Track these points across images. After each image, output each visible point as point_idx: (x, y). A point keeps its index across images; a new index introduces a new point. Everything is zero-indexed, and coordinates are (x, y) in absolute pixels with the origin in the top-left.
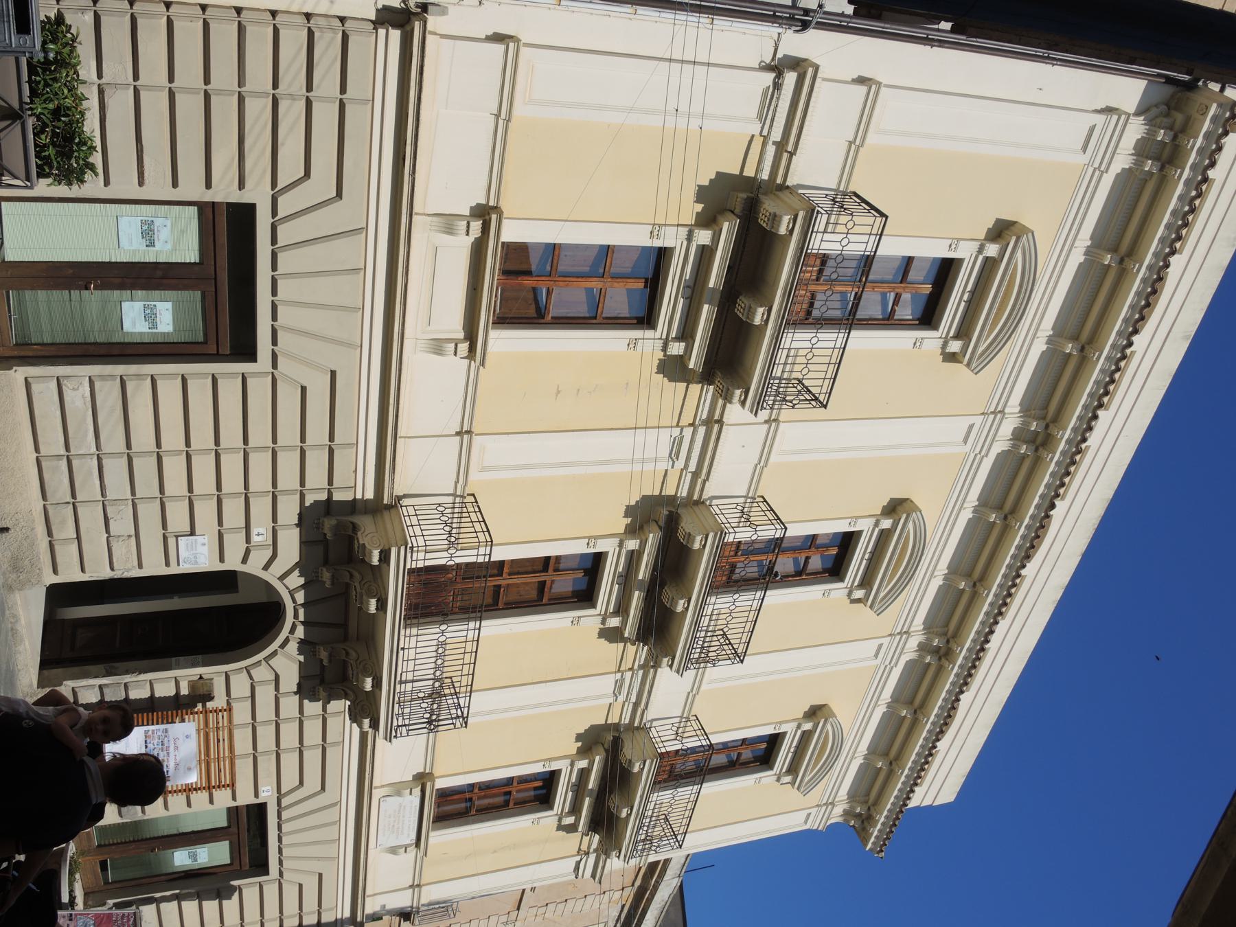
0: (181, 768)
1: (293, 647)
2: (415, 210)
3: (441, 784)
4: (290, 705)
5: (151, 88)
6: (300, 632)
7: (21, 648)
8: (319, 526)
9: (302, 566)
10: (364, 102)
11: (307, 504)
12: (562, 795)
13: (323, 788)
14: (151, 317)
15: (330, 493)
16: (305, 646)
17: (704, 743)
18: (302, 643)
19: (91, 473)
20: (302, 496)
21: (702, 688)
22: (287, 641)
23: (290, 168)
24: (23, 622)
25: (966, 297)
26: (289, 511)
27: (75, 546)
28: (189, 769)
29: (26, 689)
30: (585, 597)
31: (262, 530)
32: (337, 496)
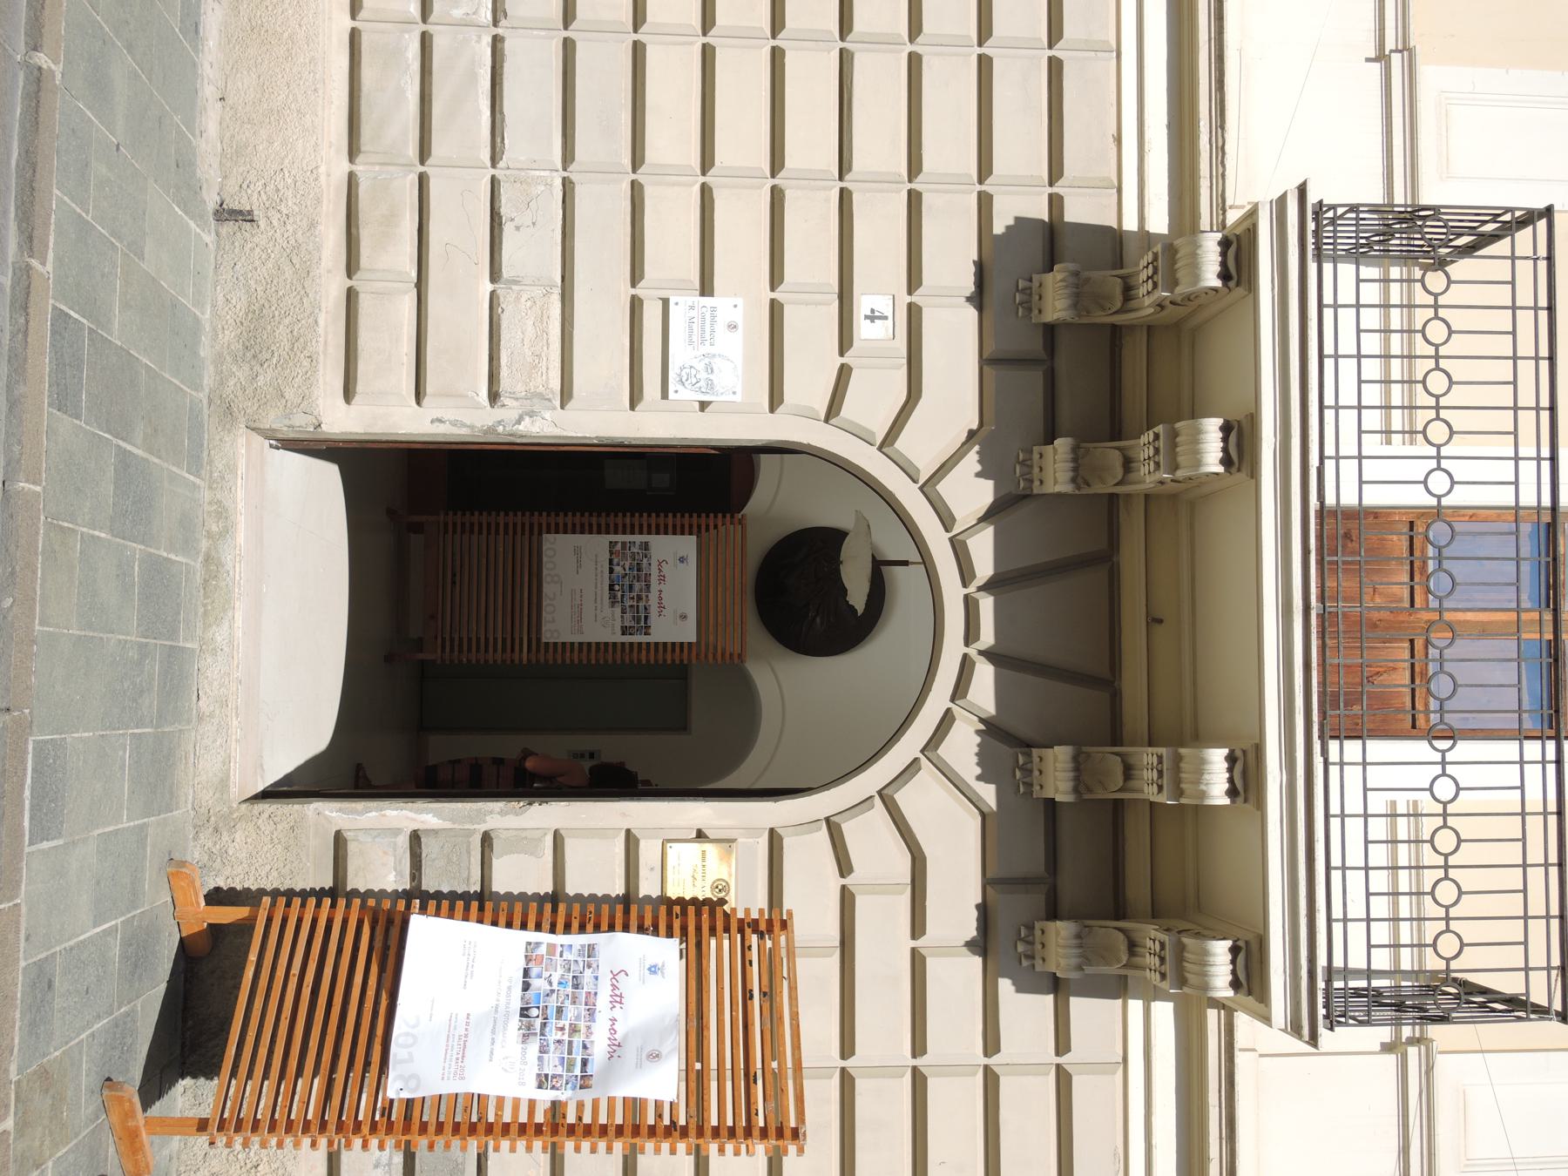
0: (630, 1053)
1: (963, 746)
2: (1237, 1045)
4: (958, 979)
6: (984, 688)
7: (220, 635)
8: (1029, 300)
9: (992, 441)
10: (1097, 48)
11: (998, 228)
14: (629, 586)
15: (1055, 202)
16: (1005, 741)
18: (992, 730)
19: (473, 77)
20: (985, 203)
22: (947, 720)
24: (241, 538)
26: (952, 259)
27: (409, 302)
28: (655, 1056)
29: (208, 798)
31: (883, 305)
32: (1075, 213)
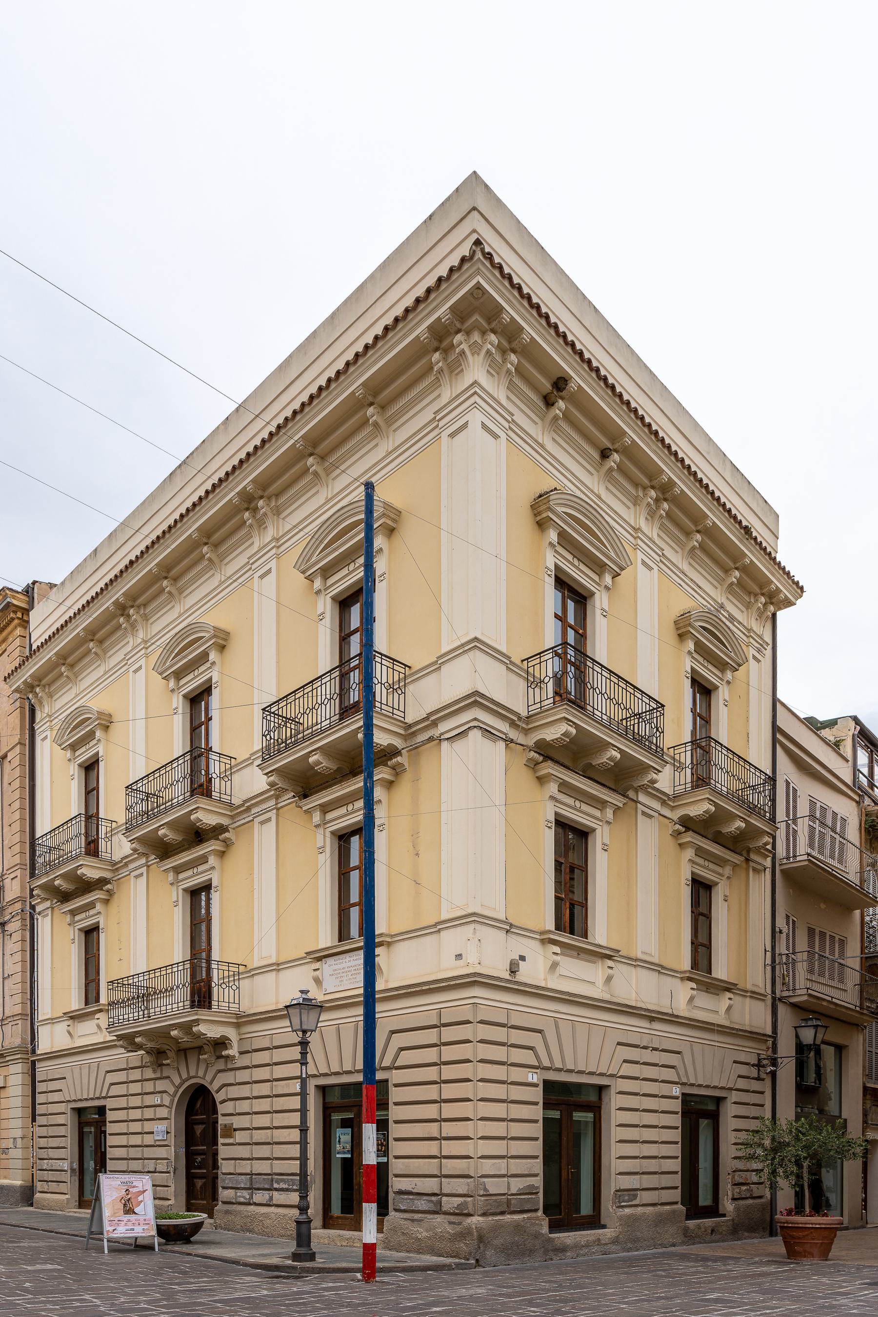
3: (551, 925)
5: (143, 1125)
12: (581, 815)
13: (540, 1031)
17: (689, 748)
21: (504, 650)
23: (526, 1057)
25: (576, 562)
30: (583, 834)
